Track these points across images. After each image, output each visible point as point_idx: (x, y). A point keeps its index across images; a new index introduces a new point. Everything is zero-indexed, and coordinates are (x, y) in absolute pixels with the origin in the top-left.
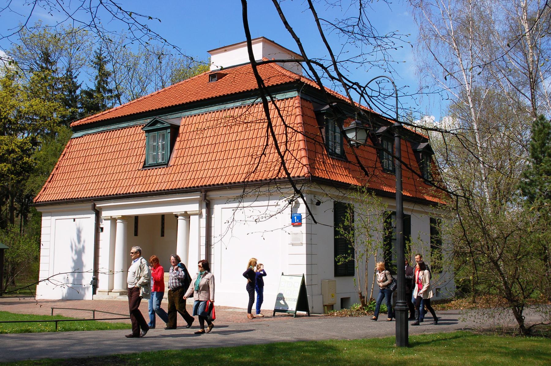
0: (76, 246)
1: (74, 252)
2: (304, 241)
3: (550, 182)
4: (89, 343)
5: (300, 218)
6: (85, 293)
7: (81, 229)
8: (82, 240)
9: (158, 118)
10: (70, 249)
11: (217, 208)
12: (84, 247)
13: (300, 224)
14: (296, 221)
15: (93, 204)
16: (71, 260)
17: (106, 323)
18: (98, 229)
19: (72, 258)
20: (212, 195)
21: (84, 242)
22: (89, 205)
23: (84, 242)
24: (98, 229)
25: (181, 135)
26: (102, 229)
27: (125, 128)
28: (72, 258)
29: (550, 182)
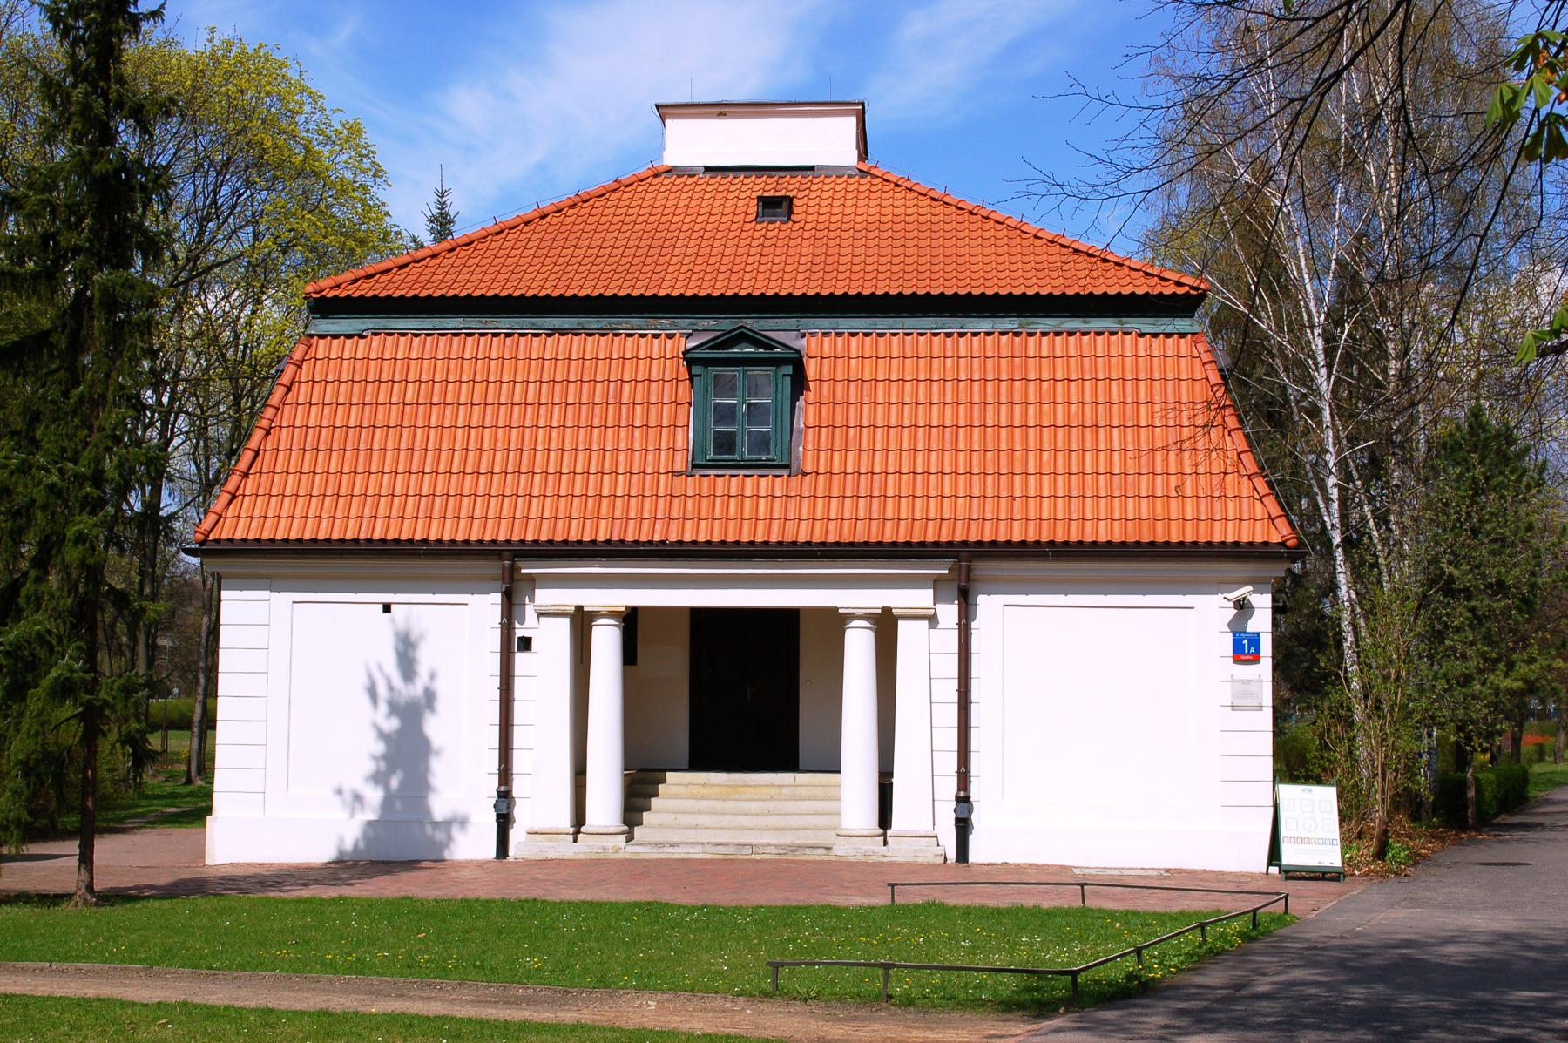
0: (391, 688)
1: (383, 708)
2: (1267, 699)
3: (5, 466)
4: (1261, 1020)
5: (1255, 640)
6: (450, 838)
7: (414, 636)
8: (423, 669)
9: (752, 323)
10: (365, 699)
11: (988, 605)
12: (430, 696)
13: (1256, 659)
14: (1244, 650)
15: (507, 566)
16: (371, 735)
17: (368, 907)
18: (513, 645)
19: (376, 726)
20: (983, 568)
21: (432, 676)
22: (494, 568)
23: (432, 676)
24: (513, 645)
25: (811, 384)
26: (526, 644)
27: (563, 332)
28: (376, 726)
29: (5, 466)
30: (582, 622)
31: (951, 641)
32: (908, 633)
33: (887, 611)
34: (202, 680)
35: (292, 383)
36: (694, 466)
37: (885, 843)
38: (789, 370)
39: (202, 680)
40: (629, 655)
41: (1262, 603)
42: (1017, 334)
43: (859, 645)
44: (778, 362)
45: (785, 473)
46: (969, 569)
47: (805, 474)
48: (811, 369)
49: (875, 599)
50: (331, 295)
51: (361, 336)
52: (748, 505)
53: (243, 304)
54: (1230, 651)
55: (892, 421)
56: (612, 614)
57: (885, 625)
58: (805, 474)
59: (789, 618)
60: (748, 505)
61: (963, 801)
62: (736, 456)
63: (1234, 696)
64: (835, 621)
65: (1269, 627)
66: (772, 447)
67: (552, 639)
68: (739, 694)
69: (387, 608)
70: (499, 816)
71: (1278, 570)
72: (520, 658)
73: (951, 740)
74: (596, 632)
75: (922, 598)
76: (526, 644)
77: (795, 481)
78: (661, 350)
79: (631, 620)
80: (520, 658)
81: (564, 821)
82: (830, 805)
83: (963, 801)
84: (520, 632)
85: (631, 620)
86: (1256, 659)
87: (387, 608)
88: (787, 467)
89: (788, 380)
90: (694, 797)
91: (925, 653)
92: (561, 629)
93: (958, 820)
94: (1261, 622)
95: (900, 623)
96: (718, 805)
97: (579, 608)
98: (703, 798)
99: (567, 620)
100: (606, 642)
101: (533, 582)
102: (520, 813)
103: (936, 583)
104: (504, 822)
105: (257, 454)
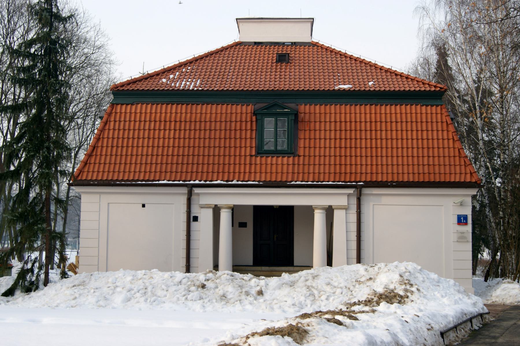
9: (280, 102)
13: (466, 224)
14: (461, 220)
18: (192, 219)
24: (192, 219)
26: (196, 219)
30: (217, 210)
31: (353, 218)
32: (339, 216)
33: (330, 207)
34: (500, 271)
35: (107, 121)
39: (500, 271)
43: (319, 218)
45: (292, 155)
49: (326, 201)
50: (122, 89)
53: (10, 44)
54: (456, 222)
56: (228, 207)
57: (329, 212)
64: (309, 210)
65: (471, 213)
67: (206, 217)
69: (144, 206)
72: (194, 224)
73: (354, 227)
75: (343, 201)
76: (196, 219)
77: (296, 158)
78: (244, 111)
80: (194, 224)
84: (193, 215)
85: (234, 210)
86: (466, 224)
87: (144, 206)
88: (293, 153)
89: (293, 121)
92: (209, 213)
94: (468, 212)
97: (216, 206)
100: (225, 217)
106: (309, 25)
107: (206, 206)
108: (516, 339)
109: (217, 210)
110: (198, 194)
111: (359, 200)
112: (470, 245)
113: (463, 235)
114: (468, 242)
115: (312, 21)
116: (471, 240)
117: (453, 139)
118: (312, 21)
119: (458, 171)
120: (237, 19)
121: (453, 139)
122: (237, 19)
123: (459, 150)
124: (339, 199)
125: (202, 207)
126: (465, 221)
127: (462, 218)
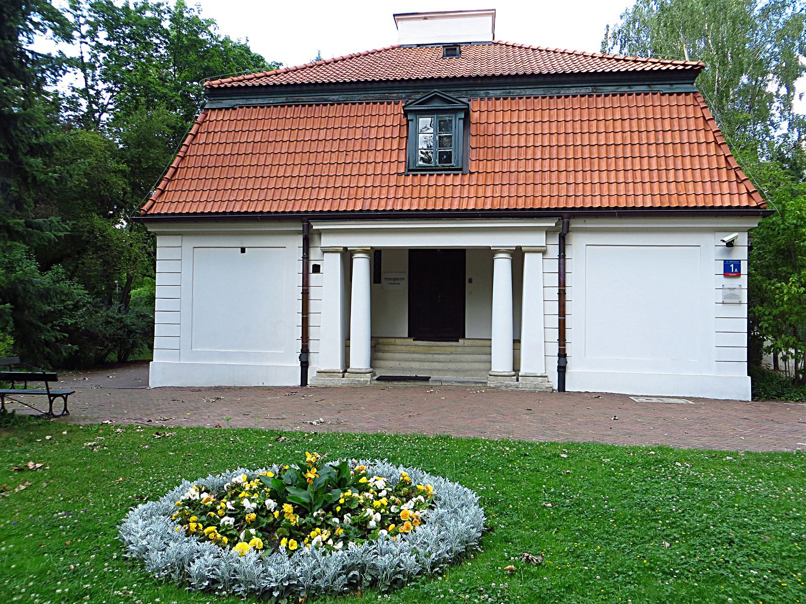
14: (730, 269)
15: (306, 224)
18: (310, 269)
20: (575, 224)
24: (310, 269)
26: (317, 269)
30: (347, 256)
32: (531, 262)
33: (519, 248)
36: (409, 170)
37: (518, 380)
38: (462, 116)
40: (376, 276)
41: (743, 240)
42: (590, 96)
43: (502, 268)
44: (455, 111)
45: (460, 172)
46: (568, 224)
47: (471, 173)
48: (475, 116)
51: (234, 109)
52: (447, 192)
55: (521, 146)
56: (364, 251)
57: (517, 256)
58: (471, 173)
59: (459, 254)
60: (447, 192)
61: (562, 355)
62: (432, 165)
63: (725, 297)
64: (488, 254)
66: (453, 160)
67: (332, 265)
68: (434, 296)
69: (243, 250)
70: (302, 363)
71: (754, 223)
74: (355, 261)
75: (539, 240)
77: (467, 177)
79: (376, 256)
80: (313, 277)
81: (338, 366)
82: (487, 343)
83: (562, 355)
85: (376, 256)
86: (739, 275)
87: (243, 250)
88: (461, 169)
89: (462, 121)
90: (409, 352)
91: (539, 273)
93: (559, 367)
94: (741, 254)
95: (526, 255)
96: (423, 356)
97: (345, 248)
98: (414, 353)
99: (339, 255)
100: (361, 267)
101: (320, 233)
102: (312, 358)
103: (549, 232)
104: (305, 365)
105: (176, 169)
106: (490, 18)
107: (331, 249)
108: (2, 306)
109: (347, 256)
110: (320, 233)
111: (562, 257)
112: (744, 311)
113: (732, 291)
114: (740, 303)
115: (492, 13)
116: (745, 299)
117: (716, 142)
118: (492, 13)
119: (726, 191)
120: (394, 15)
121: (716, 142)
122: (394, 15)
123: (726, 158)
124: (530, 239)
125: (325, 251)
126: (736, 270)
127: (732, 265)
